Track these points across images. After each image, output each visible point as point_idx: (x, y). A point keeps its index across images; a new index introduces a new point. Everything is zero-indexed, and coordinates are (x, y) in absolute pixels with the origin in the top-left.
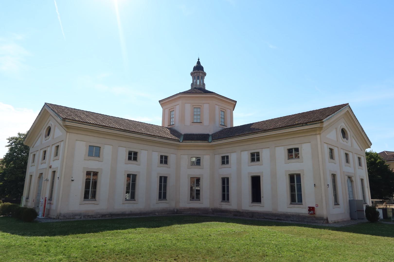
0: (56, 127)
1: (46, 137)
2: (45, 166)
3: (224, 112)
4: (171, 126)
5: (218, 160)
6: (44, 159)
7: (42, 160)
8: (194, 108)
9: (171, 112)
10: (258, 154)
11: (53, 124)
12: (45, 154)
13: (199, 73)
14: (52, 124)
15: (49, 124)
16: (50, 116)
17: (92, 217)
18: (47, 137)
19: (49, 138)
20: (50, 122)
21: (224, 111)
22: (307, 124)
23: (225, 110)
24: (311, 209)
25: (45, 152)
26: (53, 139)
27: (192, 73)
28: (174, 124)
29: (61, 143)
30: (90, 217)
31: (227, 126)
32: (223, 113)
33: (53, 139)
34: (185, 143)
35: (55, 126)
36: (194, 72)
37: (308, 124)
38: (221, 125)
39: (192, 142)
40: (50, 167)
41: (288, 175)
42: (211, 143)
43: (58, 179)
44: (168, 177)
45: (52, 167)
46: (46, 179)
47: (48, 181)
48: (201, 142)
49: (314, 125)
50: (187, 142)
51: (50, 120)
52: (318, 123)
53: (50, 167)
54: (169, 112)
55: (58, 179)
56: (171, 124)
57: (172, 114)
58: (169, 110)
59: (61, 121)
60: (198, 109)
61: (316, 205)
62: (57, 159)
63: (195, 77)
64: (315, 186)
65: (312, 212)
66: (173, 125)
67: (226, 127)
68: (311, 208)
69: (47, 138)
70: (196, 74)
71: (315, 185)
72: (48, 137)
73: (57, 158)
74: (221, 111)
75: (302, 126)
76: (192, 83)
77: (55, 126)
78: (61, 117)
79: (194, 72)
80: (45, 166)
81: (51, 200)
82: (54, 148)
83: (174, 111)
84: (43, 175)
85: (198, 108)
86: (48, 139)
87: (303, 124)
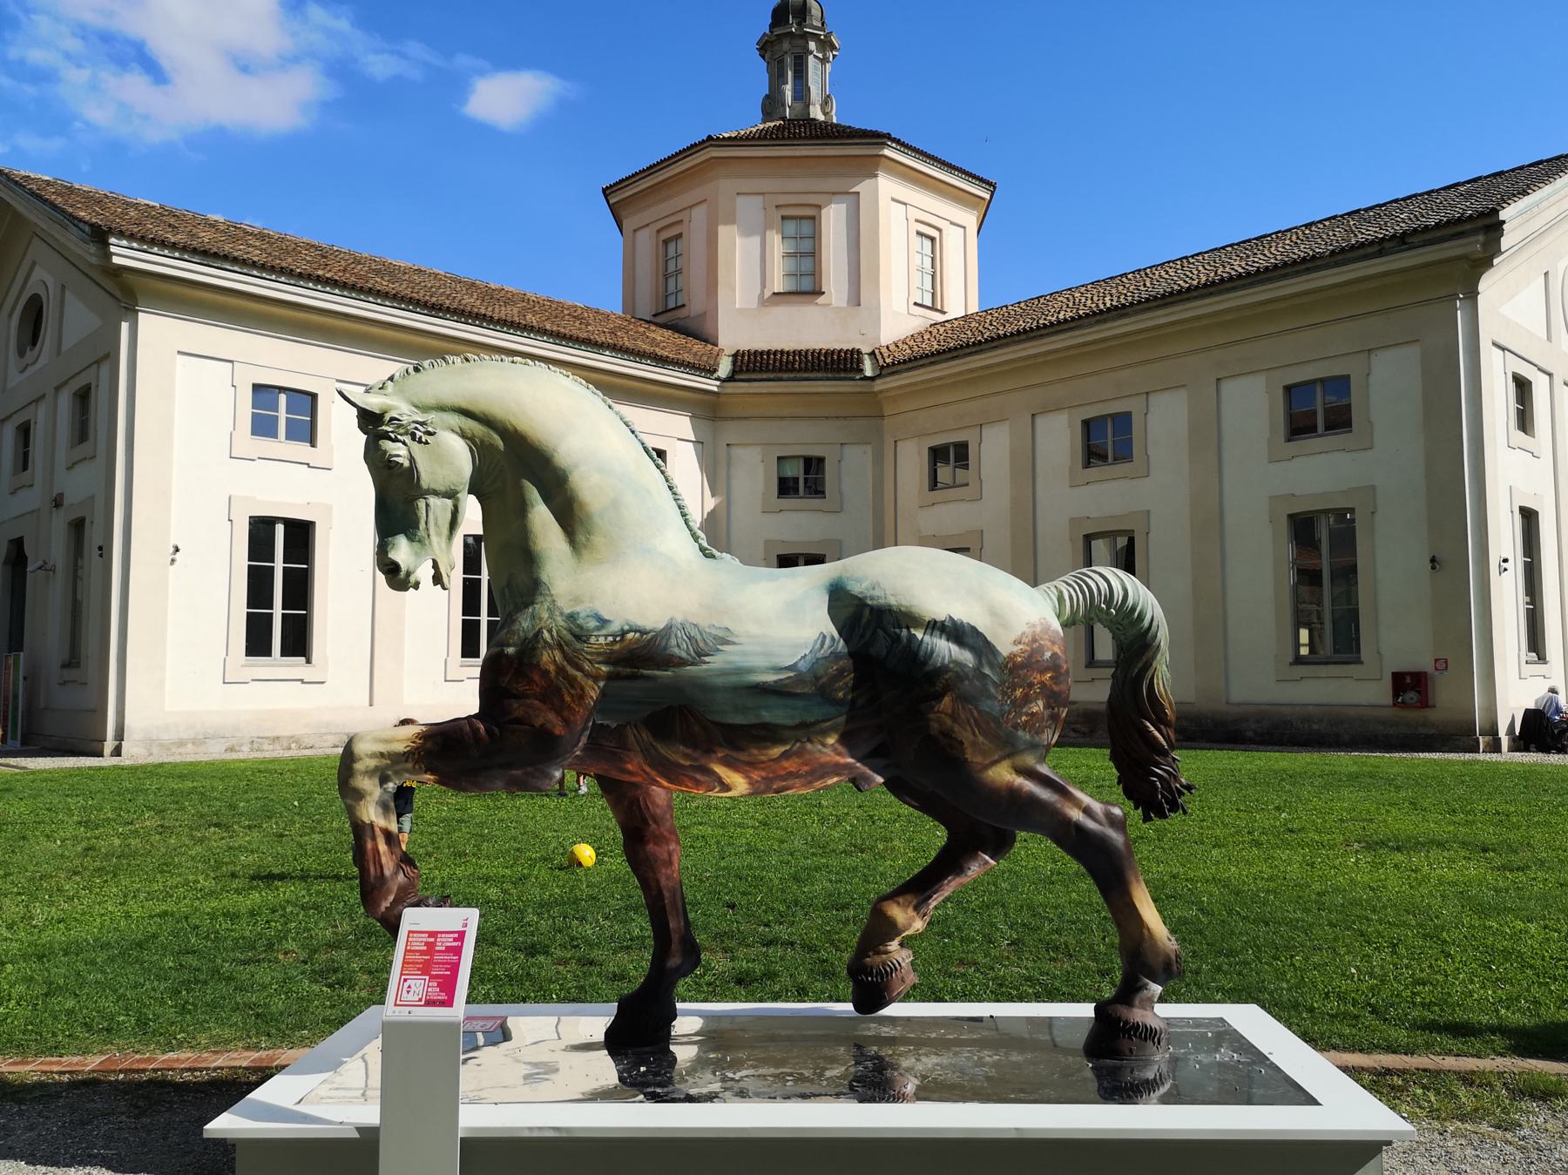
0: (68, 294)
1: (21, 353)
2: (32, 499)
3: (932, 239)
4: (670, 314)
5: (912, 462)
6: (25, 468)
7: (15, 473)
8: (784, 218)
9: (666, 242)
10: (1123, 422)
11: (50, 281)
12: (26, 443)
13: (801, 42)
14: (45, 283)
15: (30, 282)
16: (32, 237)
17: (293, 746)
18: (28, 352)
19: (37, 359)
20: (39, 274)
21: (935, 233)
22: (1410, 240)
23: (940, 230)
24: (1410, 685)
25: (25, 431)
26: (59, 353)
27: (767, 41)
28: (683, 306)
29: (99, 367)
30: (285, 744)
31: (945, 310)
32: (928, 243)
33: (59, 353)
34: (747, 384)
35: (63, 287)
36: (778, 31)
37: (1415, 240)
38: (915, 304)
39: (780, 380)
40: (55, 500)
41: (1284, 520)
42: (878, 382)
43: (101, 556)
44: (1283, 440)
45: (66, 502)
46: (40, 563)
47: (54, 571)
48: (828, 379)
49: (1446, 245)
50: (755, 380)
51: (34, 264)
52: (1474, 232)
53: (58, 502)
54: (657, 244)
55: (101, 556)
56: (671, 305)
57: (672, 253)
58: (658, 231)
59: (81, 244)
60: (803, 221)
61: (1436, 660)
62: (85, 458)
63: (781, 62)
64: (1433, 568)
65: (1411, 696)
66: (677, 308)
67: (940, 318)
68: (1408, 680)
69: (30, 355)
70: (786, 45)
71: (1433, 560)
72: (31, 350)
73: (85, 448)
74: (919, 233)
75: (1380, 254)
76: (767, 97)
77: (63, 287)
78: (81, 225)
79: (778, 31)
80: (32, 499)
81: (78, 665)
82: (65, 401)
83: (680, 236)
84: (28, 549)
85: (802, 218)
86: (32, 364)
87: (1387, 245)
